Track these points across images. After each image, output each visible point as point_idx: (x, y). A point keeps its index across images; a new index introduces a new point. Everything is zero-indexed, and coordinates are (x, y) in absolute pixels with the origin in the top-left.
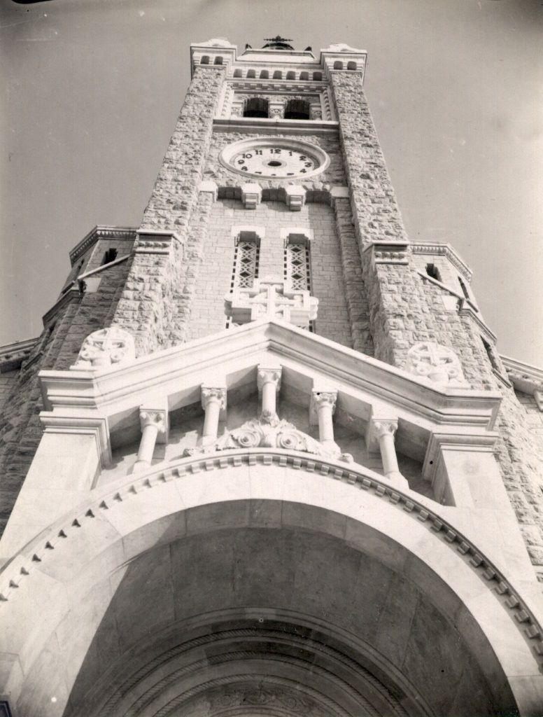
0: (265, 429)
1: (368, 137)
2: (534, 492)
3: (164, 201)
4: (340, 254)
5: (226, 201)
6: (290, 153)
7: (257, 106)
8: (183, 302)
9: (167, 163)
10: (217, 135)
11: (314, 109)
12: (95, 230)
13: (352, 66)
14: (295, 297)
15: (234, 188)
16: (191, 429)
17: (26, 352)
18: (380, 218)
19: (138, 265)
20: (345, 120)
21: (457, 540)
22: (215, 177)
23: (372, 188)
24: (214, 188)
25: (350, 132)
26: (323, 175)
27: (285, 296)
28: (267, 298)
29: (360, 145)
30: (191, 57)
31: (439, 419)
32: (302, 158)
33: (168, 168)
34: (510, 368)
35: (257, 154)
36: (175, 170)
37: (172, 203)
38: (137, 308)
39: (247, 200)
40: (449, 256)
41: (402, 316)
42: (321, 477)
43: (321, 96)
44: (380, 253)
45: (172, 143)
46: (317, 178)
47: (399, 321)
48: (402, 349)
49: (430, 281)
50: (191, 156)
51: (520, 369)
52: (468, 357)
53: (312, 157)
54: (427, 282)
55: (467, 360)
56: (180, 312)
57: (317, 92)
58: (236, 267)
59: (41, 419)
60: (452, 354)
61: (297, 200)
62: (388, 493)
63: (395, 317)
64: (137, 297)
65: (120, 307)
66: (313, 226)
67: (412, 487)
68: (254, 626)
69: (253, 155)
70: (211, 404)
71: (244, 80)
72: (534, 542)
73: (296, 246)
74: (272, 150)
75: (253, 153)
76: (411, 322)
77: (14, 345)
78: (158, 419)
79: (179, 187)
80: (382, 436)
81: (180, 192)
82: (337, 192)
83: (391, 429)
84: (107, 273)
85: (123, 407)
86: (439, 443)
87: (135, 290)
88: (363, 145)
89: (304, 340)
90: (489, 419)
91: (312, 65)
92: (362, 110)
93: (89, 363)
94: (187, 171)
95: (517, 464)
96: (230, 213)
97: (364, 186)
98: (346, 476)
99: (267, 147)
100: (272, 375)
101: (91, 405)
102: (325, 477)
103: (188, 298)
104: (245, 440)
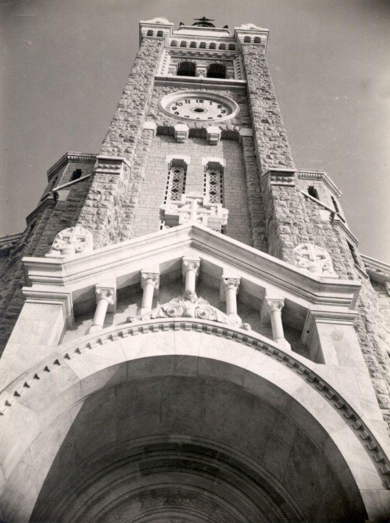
0: (187, 304)
1: (268, 92)
2: (383, 355)
3: (118, 135)
4: (245, 177)
8: (129, 210)
9: (120, 107)
10: (158, 88)
12: (66, 155)
13: (257, 40)
14: (211, 208)
15: (169, 127)
16: (132, 303)
17: (13, 243)
19: (97, 182)
22: (155, 119)
24: (154, 127)
27: (205, 207)
28: (190, 208)
29: (262, 98)
30: (140, 31)
32: (219, 107)
33: (121, 111)
34: (367, 264)
35: (186, 103)
36: (126, 113)
37: (123, 137)
40: (325, 181)
43: (234, 61)
44: (274, 177)
45: (124, 93)
49: (310, 199)
50: (138, 103)
51: (374, 265)
53: (226, 106)
54: (309, 199)
55: (336, 257)
56: (127, 217)
60: (325, 253)
61: (215, 137)
62: (276, 354)
63: (284, 225)
65: (83, 212)
66: (226, 157)
67: (293, 349)
68: (175, 447)
70: (148, 285)
71: (178, 49)
72: (381, 391)
73: (213, 171)
74: (197, 100)
75: (183, 102)
76: (296, 228)
78: (108, 295)
79: (129, 125)
81: (129, 129)
82: (244, 132)
84: (74, 187)
86: (314, 317)
87: (95, 200)
88: (264, 98)
90: (351, 300)
91: (228, 39)
92: (264, 72)
93: (59, 252)
94: (135, 114)
95: (371, 334)
96: (165, 144)
97: (264, 128)
98: (245, 340)
99: (194, 98)
101: (60, 283)
103: (133, 207)
104: (172, 312)
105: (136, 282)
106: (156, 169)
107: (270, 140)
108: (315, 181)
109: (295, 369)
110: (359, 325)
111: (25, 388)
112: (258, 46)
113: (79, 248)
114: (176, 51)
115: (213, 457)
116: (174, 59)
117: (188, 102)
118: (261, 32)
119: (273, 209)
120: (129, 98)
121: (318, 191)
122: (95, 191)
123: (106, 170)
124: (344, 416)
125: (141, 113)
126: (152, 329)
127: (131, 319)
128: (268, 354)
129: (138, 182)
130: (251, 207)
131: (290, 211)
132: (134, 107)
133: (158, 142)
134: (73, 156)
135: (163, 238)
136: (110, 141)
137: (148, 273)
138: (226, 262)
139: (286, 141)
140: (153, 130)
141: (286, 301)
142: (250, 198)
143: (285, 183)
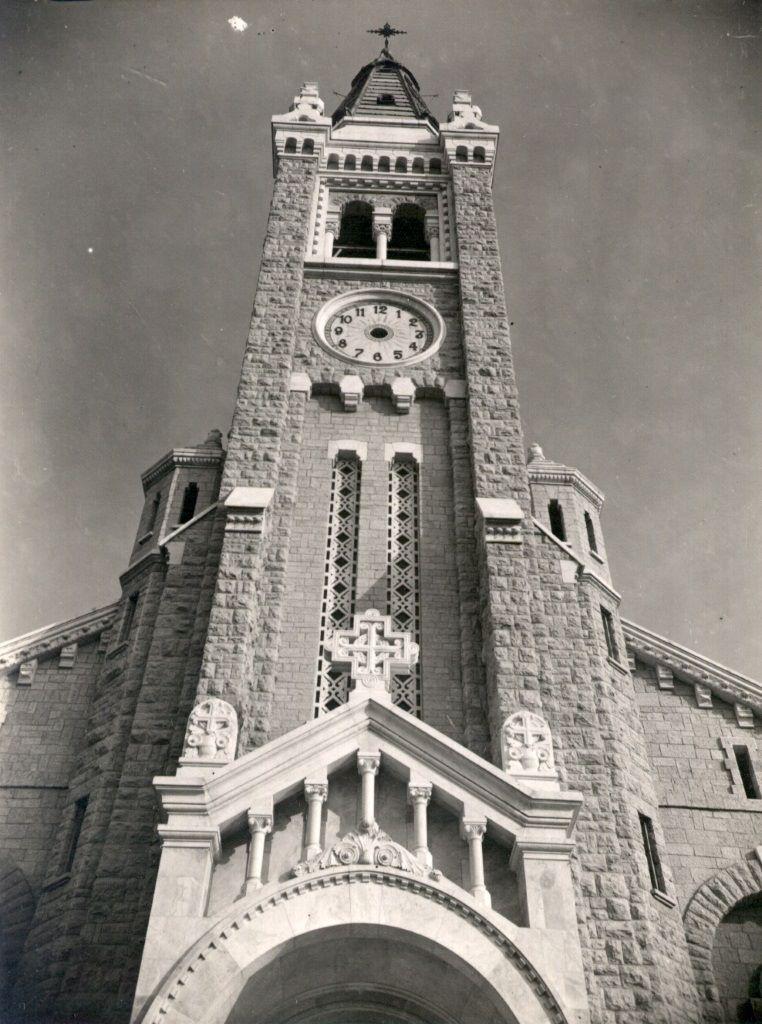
1: (492, 296)
2: (630, 824)
3: (250, 420)
4: (451, 485)
5: (322, 398)
6: (399, 312)
7: (358, 209)
10: (312, 282)
11: (429, 221)
13: (479, 154)
14: (396, 642)
16: (295, 813)
17: (105, 623)
18: (499, 445)
20: (467, 263)
21: (526, 968)
23: (491, 392)
24: (307, 386)
25: (471, 287)
26: (437, 359)
27: (386, 639)
28: (366, 643)
29: (482, 313)
31: (525, 821)
32: (412, 323)
33: (252, 361)
34: (631, 637)
35: (358, 315)
36: (261, 365)
37: (259, 425)
38: (230, 620)
39: (347, 402)
40: (576, 485)
41: (509, 626)
42: (413, 895)
44: (491, 529)
45: (254, 314)
46: (429, 363)
47: (505, 633)
48: (505, 674)
49: (549, 538)
50: (278, 338)
52: (580, 653)
53: (424, 320)
54: (547, 540)
56: (273, 591)
57: (435, 191)
58: (335, 481)
59: (160, 833)
60: (546, 731)
61: (405, 401)
62: (472, 916)
63: (502, 628)
64: (230, 603)
67: (495, 906)
69: (353, 317)
71: (342, 172)
74: (376, 308)
75: (352, 312)
76: (518, 633)
77: (90, 614)
78: (265, 825)
79: (267, 395)
80: (472, 840)
81: (268, 403)
82: (451, 389)
83: (480, 832)
85: (230, 813)
87: (228, 592)
88: (486, 314)
89: (401, 722)
91: (428, 147)
92: (488, 242)
94: (275, 365)
95: (617, 789)
96: (326, 417)
97: (484, 390)
98: (435, 895)
99: (370, 302)
100: (371, 763)
101: (202, 812)
102: (417, 896)
104: (346, 857)
105: (300, 790)
106: (314, 474)
107: (492, 418)
108: (561, 488)
109: (493, 939)
110: (599, 784)
111: (179, 986)
112: (480, 168)
113: (221, 742)
114: (338, 178)
115: (401, 1009)
116: (335, 194)
117: (360, 313)
118: (485, 136)
119: (488, 592)
120: (264, 326)
121: (563, 510)
122: (228, 574)
123: (240, 527)
124: (545, 1006)
125: (285, 364)
126: (321, 883)
127: (296, 873)
128: (461, 916)
129: (287, 515)
130: (459, 557)
131: (512, 598)
132: (274, 349)
133: (315, 412)
134: (182, 456)
135: (329, 724)
136: (240, 434)
137: (313, 785)
138: (413, 757)
139: (516, 418)
140: (306, 393)
141: (490, 824)
142: (459, 540)
143: (508, 539)
